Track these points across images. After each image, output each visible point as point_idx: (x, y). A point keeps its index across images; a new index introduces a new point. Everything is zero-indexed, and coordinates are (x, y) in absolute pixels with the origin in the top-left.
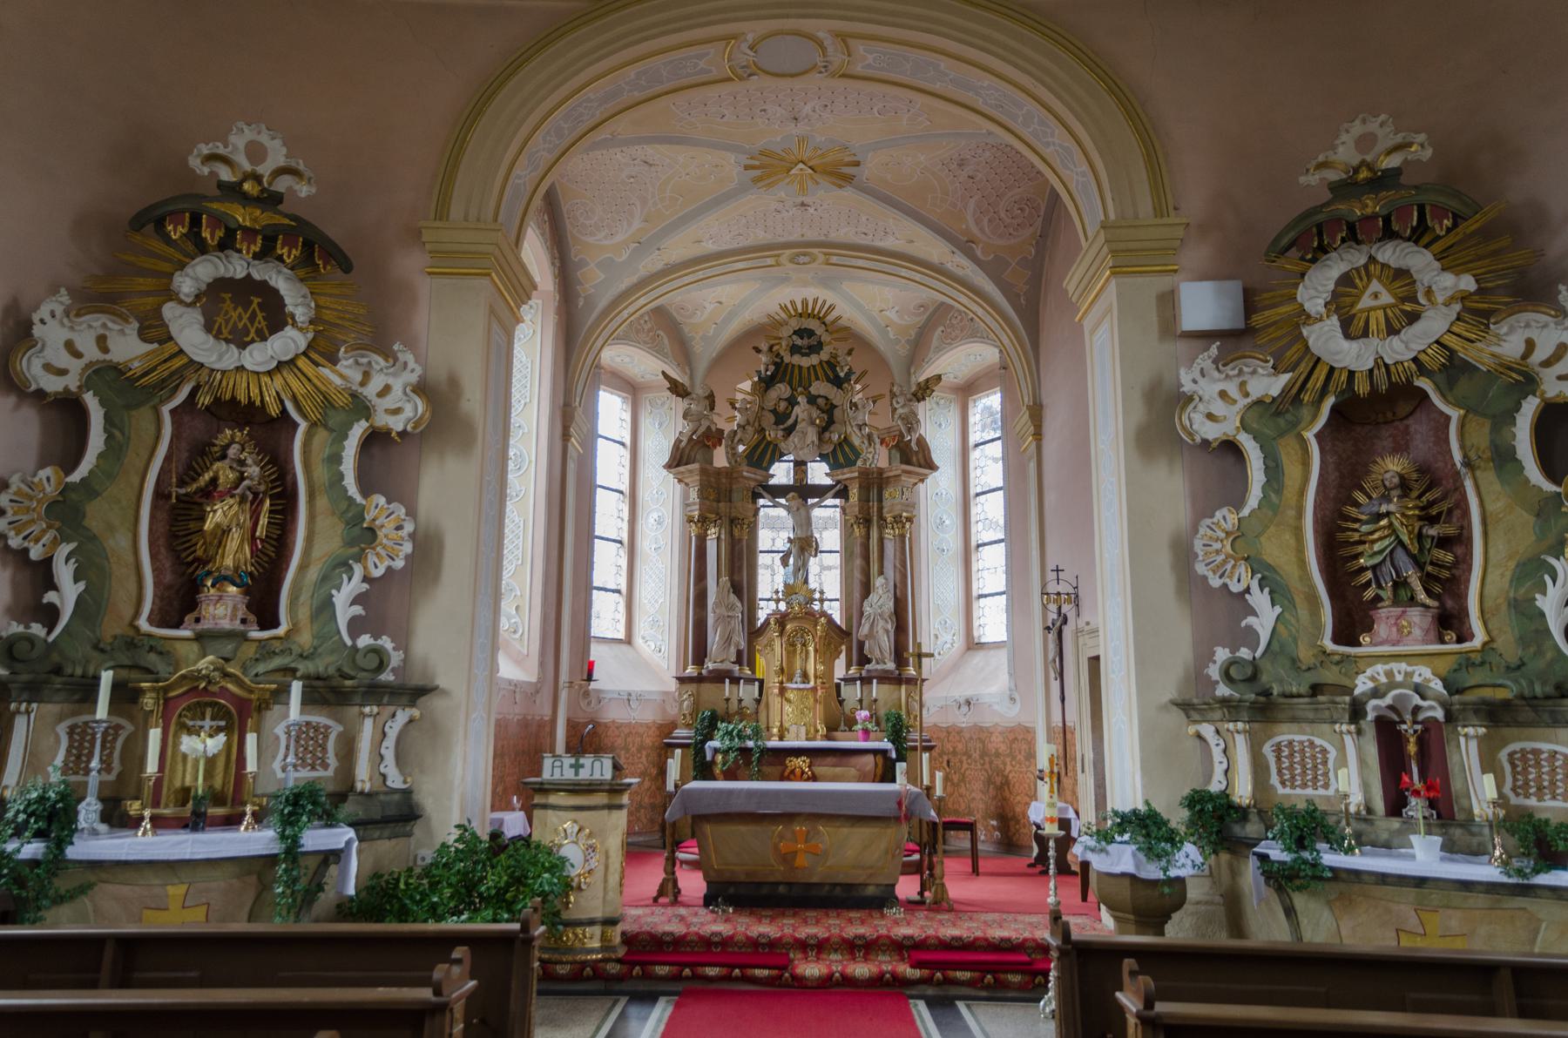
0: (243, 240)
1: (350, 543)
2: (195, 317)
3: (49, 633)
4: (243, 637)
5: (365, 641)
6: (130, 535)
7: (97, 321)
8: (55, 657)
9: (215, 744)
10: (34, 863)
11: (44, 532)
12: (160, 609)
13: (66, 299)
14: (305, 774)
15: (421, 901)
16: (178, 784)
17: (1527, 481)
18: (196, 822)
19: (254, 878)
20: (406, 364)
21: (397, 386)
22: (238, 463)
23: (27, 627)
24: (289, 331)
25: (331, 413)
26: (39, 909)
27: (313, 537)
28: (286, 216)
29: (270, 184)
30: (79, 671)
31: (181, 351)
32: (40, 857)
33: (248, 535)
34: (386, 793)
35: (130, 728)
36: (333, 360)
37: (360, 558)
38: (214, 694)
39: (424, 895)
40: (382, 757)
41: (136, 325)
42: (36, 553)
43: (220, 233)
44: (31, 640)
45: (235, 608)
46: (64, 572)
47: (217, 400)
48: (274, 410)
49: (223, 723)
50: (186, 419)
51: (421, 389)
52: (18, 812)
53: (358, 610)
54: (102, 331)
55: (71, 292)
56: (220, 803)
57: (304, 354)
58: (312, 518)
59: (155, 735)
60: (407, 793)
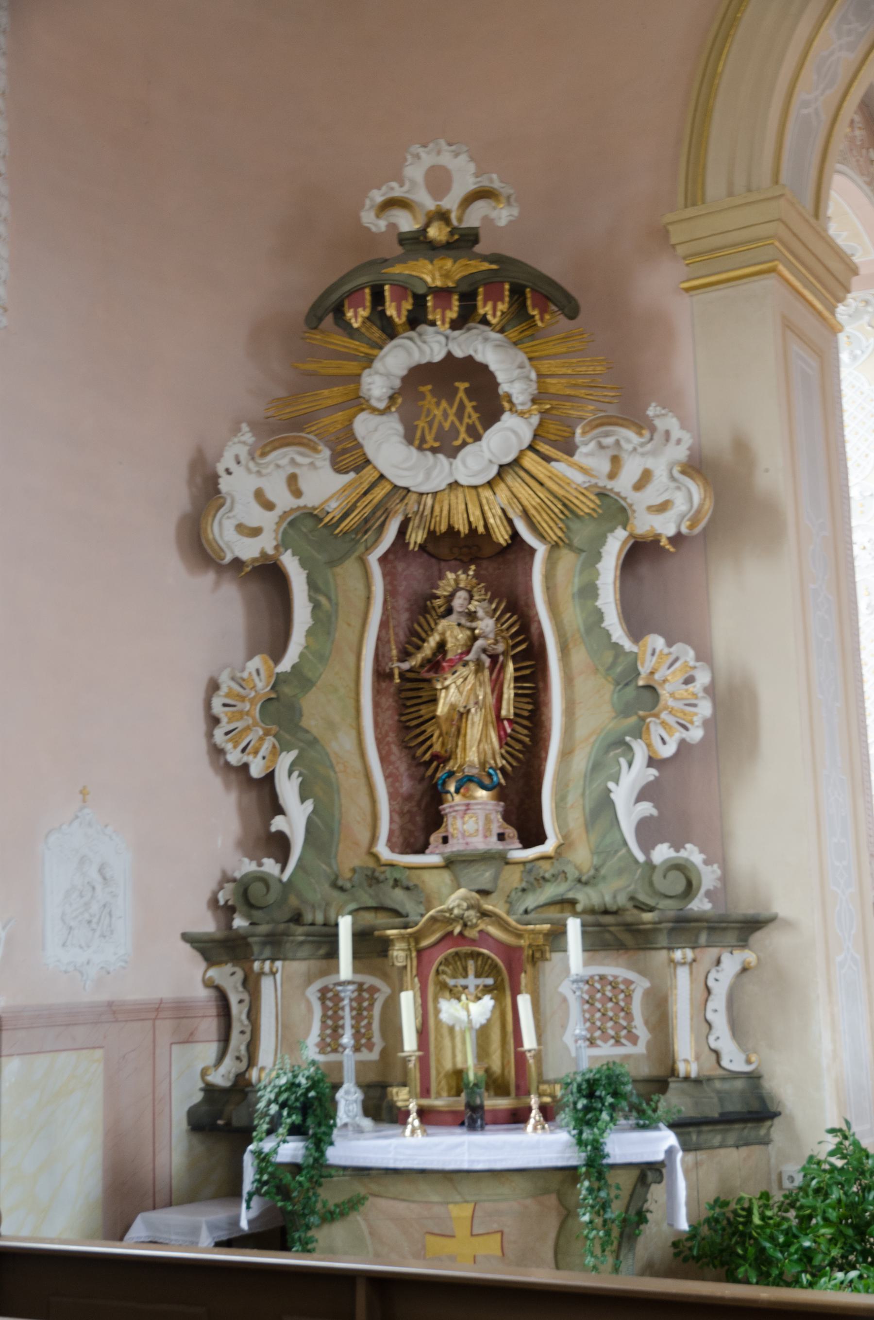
0: (435, 307)
1: (625, 711)
2: (393, 425)
3: (283, 869)
4: (503, 859)
5: (662, 853)
6: (353, 733)
7: (284, 458)
8: (293, 901)
9: (481, 1009)
10: (295, 1168)
11: (261, 739)
12: (402, 828)
13: (248, 437)
14: (607, 1051)
15: (787, 1245)
16: (448, 1066)
17: (608, 635)
18: (473, 1118)
19: (552, 1200)
20: (667, 434)
21: (660, 469)
22: (469, 620)
23: (260, 865)
24: (508, 420)
25: (575, 525)
26: (308, 1227)
27: (574, 707)
28: (485, 258)
29: (460, 220)
30: (320, 918)
31: (382, 477)
32: (299, 1160)
33: (492, 717)
34: (723, 1079)
35: (385, 990)
36: (569, 449)
37: (639, 731)
38: (473, 942)
39: (791, 1236)
40: (709, 1025)
41: (326, 453)
42: (257, 771)
43: (408, 305)
44: (263, 879)
45: (488, 820)
46: (288, 789)
47: (432, 534)
48: (502, 536)
49: (490, 981)
50: (400, 566)
51: (696, 467)
52: (269, 1103)
53: (647, 808)
54: (291, 470)
55: (254, 426)
56: (492, 1096)
57: (531, 448)
58: (568, 681)
59: (407, 1000)
60: (754, 1078)
